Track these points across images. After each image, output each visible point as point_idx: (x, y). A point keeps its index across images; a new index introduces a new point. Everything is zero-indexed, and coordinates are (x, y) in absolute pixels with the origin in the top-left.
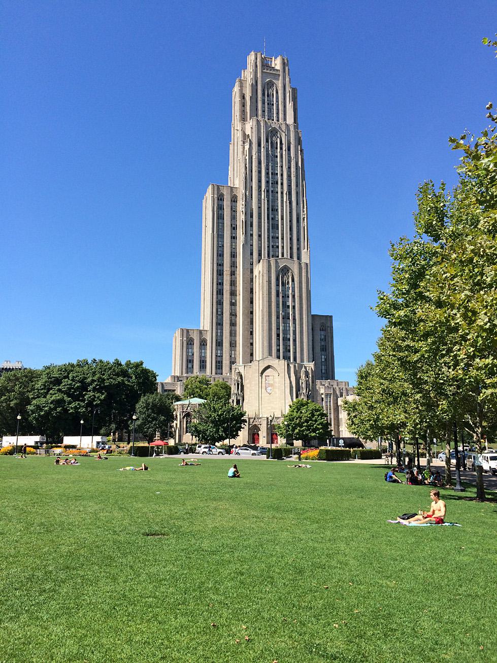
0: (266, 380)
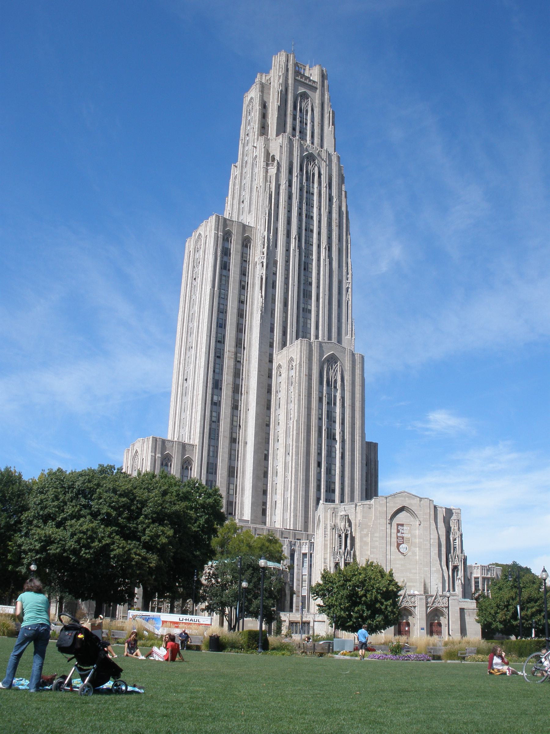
0: (398, 531)
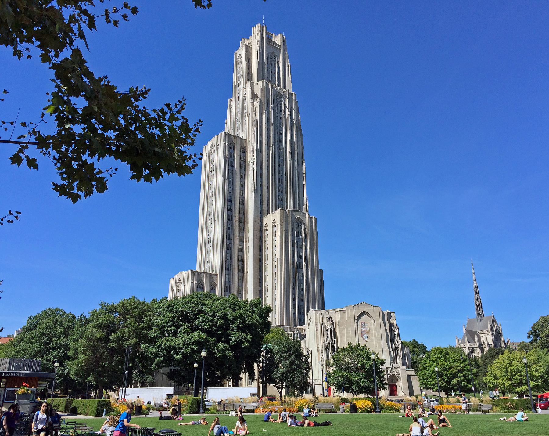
0: (362, 327)
